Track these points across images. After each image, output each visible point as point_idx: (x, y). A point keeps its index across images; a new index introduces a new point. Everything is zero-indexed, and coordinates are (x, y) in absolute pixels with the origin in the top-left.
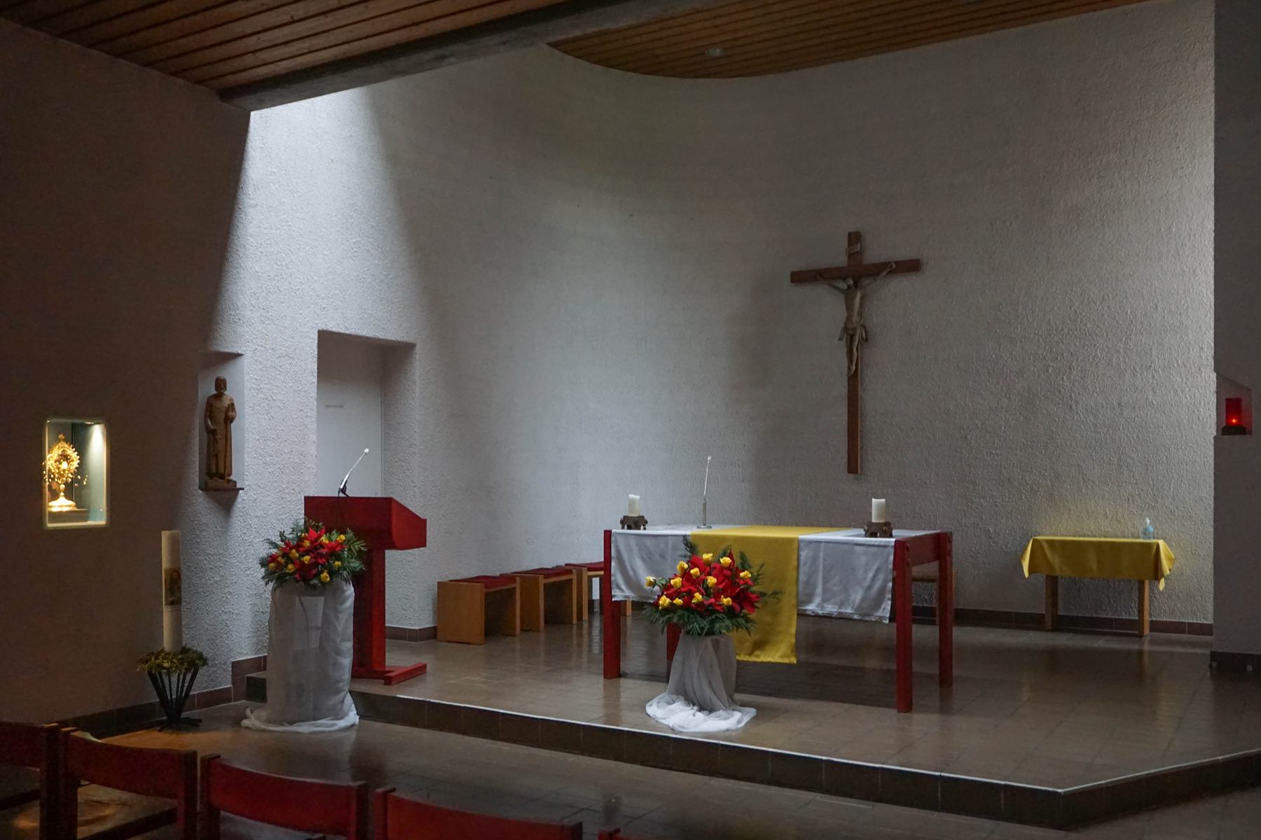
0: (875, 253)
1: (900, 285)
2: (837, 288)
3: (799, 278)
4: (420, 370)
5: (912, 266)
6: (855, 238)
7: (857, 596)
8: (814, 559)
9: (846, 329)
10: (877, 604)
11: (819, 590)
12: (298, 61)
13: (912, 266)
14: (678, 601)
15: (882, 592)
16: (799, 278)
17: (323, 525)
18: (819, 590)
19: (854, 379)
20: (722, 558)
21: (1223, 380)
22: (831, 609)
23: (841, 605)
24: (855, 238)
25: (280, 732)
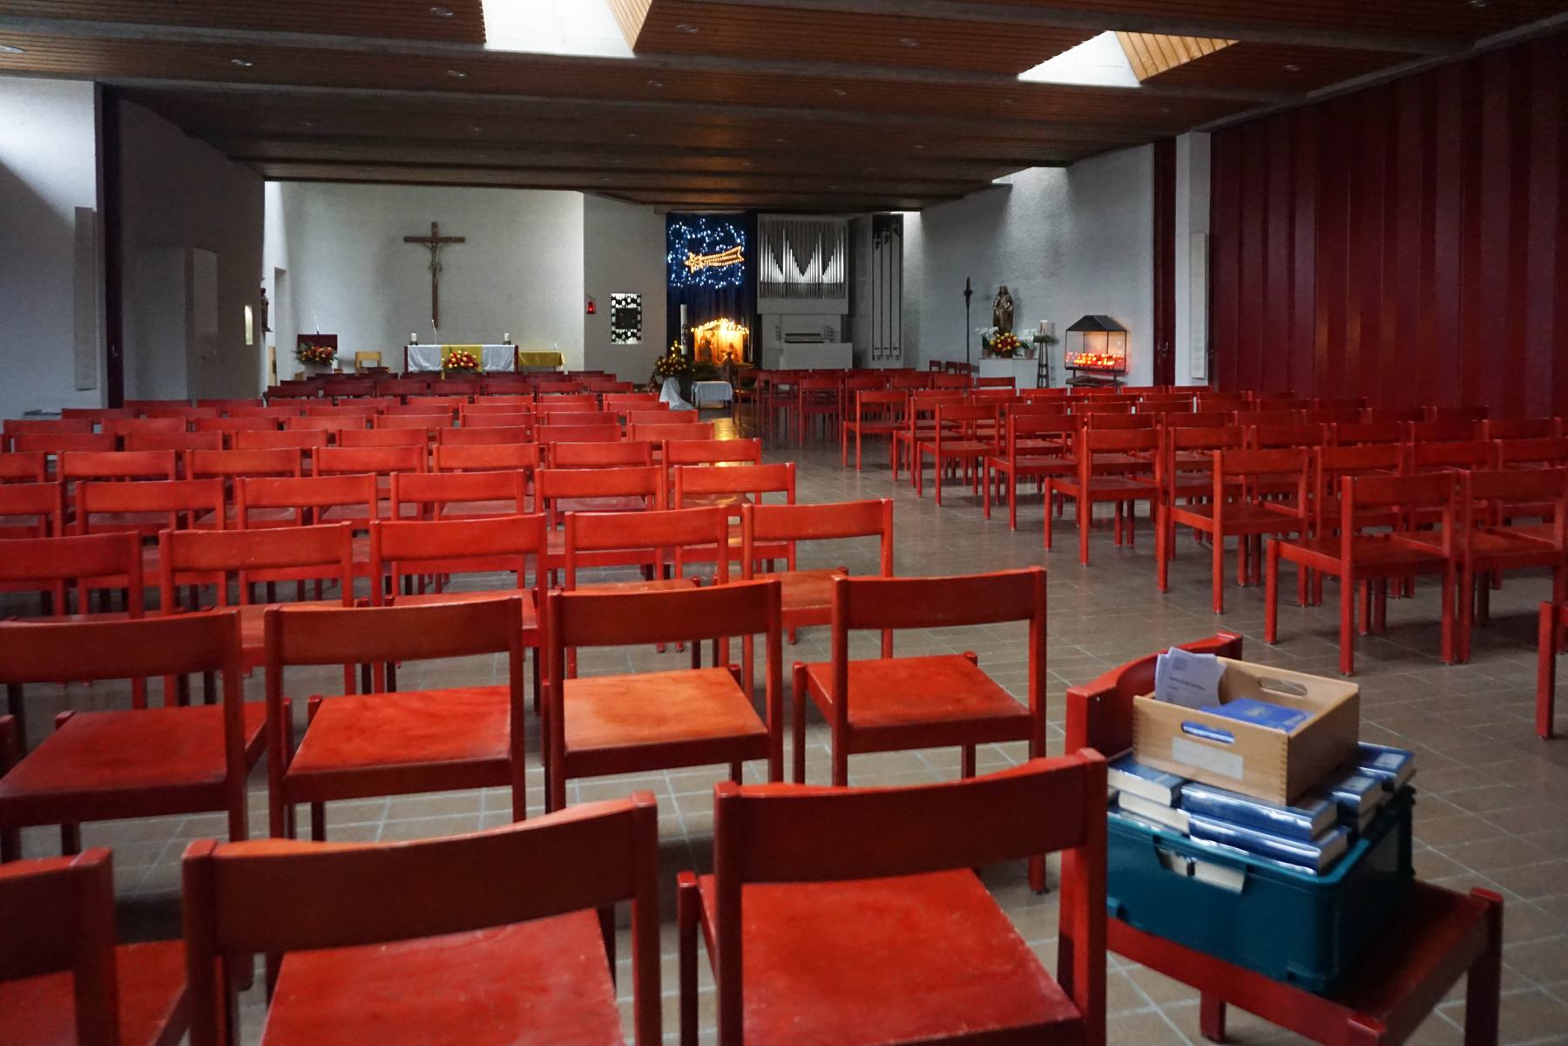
0: (443, 233)
1: (456, 248)
2: (428, 247)
3: (407, 240)
4: (287, 277)
5: (461, 240)
6: (434, 225)
7: (502, 364)
8: (487, 354)
9: (432, 264)
10: (509, 366)
11: (490, 362)
12: (322, 154)
13: (461, 240)
14: (456, 365)
15: (511, 362)
16: (407, 240)
17: (683, 369)
18: (490, 362)
19: (435, 287)
20: (860, 389)
21: (587, 295)
22: (494, 368)
23: (497, 366)
24: (434, 225)
25: (95, 376)
